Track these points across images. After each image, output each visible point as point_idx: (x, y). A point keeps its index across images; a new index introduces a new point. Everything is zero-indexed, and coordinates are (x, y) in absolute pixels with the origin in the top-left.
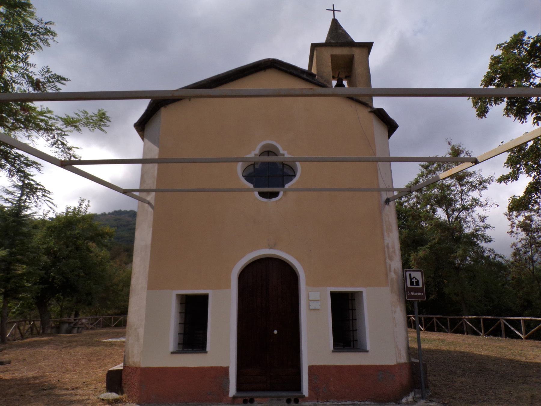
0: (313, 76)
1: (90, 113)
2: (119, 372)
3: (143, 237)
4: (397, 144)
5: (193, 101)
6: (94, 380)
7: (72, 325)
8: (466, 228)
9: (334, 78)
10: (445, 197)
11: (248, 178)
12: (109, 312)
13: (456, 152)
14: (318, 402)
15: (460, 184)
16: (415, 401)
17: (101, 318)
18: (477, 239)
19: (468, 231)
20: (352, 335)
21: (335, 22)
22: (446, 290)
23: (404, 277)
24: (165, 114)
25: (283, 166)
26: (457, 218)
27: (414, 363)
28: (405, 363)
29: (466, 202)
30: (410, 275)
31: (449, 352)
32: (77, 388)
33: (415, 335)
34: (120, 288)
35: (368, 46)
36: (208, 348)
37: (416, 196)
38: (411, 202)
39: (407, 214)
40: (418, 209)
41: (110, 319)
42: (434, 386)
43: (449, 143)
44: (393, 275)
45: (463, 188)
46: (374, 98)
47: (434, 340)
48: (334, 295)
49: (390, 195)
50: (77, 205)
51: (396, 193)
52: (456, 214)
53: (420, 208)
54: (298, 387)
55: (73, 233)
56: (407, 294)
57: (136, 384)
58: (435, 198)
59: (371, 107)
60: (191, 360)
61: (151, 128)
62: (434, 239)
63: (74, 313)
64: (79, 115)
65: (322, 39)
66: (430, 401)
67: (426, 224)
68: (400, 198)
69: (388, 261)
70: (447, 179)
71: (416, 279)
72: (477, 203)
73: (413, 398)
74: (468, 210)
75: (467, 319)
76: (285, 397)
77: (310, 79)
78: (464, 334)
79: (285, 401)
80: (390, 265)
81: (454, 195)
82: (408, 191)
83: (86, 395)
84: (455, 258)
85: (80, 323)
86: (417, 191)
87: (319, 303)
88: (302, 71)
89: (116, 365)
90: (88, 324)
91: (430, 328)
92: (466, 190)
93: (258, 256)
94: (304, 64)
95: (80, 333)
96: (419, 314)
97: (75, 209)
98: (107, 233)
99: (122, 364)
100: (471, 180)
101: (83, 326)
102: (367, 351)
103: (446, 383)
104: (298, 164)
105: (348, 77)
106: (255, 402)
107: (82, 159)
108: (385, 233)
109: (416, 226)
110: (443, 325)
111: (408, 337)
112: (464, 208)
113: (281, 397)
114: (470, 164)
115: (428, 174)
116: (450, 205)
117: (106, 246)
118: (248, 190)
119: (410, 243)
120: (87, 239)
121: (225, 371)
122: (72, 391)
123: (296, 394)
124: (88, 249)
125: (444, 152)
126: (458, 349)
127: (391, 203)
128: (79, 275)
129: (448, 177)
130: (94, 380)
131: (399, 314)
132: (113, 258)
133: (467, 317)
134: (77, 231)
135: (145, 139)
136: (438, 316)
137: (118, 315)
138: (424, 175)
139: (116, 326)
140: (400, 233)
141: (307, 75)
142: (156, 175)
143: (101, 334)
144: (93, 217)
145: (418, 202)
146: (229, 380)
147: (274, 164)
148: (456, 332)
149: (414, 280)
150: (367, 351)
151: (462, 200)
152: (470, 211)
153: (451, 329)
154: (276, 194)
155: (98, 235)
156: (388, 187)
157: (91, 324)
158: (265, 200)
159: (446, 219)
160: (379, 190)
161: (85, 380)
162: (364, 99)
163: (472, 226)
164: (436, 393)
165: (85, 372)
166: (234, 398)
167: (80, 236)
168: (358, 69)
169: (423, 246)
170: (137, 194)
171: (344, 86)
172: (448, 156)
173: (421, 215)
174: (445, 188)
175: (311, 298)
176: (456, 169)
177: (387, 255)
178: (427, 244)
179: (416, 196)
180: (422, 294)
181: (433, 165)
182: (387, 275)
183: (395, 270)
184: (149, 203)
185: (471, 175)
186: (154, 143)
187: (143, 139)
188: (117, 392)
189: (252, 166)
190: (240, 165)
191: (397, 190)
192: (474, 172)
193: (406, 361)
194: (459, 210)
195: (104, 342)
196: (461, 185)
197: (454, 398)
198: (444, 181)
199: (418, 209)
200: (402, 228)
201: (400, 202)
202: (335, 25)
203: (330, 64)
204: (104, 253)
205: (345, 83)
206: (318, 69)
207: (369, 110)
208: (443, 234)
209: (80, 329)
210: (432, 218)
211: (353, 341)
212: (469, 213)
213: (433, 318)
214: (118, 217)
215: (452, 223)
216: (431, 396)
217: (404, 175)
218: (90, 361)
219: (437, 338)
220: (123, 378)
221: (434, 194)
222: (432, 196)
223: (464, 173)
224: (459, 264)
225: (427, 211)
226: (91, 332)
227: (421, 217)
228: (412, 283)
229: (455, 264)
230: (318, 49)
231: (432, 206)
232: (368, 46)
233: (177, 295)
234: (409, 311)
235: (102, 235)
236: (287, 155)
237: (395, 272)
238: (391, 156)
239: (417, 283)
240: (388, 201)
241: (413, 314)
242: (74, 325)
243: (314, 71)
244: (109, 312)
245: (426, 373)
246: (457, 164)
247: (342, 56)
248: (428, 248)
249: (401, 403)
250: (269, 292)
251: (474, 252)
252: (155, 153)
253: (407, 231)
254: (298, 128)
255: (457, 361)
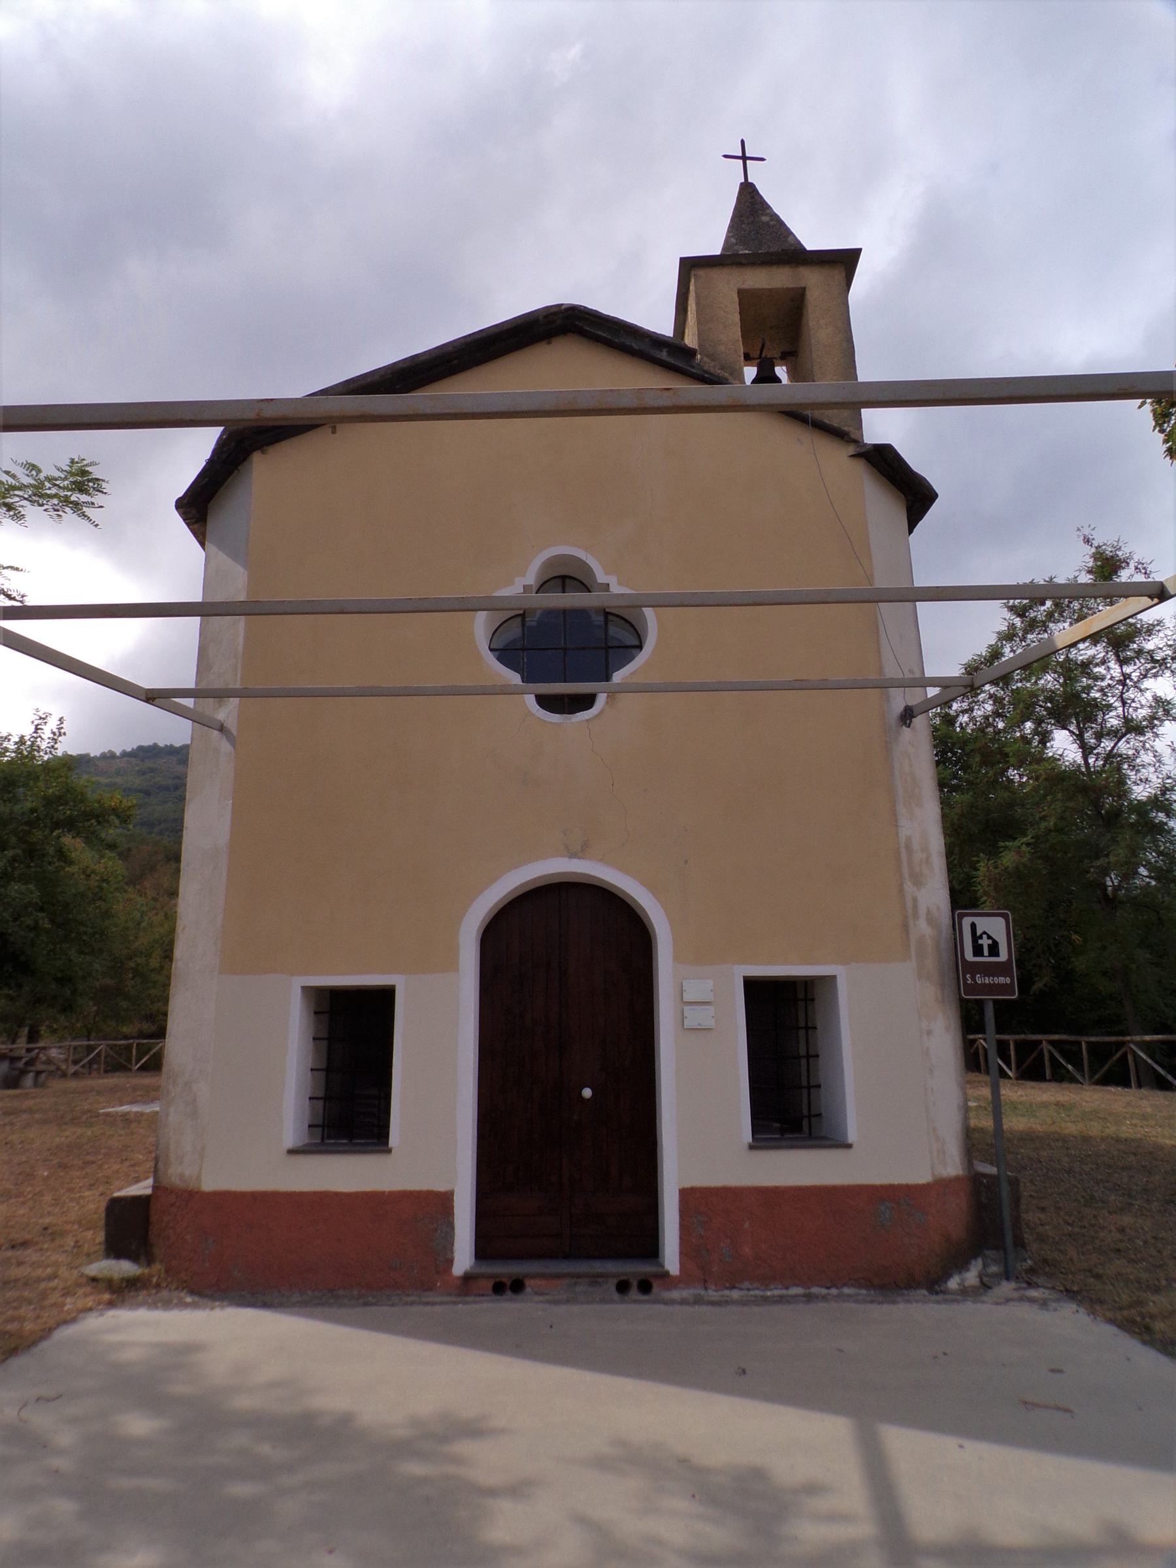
0: (690, 353)
1: (48, 470)
2: (141, 1203)
3: (207, 824)
4: (932, 552)
5: (350, 432)
6: (73, 1223)
7: (20, 1064)
8: (1135, 783)
9: (748, 358)
10: (1077, 696)
11: (506, 654)
12: (125, 1030)
13: (1107, 565)
14: (706, 1289)
15: (1118, 656)
16: (985, 1286)
17: (102, 1046)
18: (1168, 816)
19: (1140, 793)
20: (805, 1101)
21: (748, 192)
22: (1080, 964)
23: (954, 929)
24: (264, 471)
25: (606, 621)
26: (1110, 756)
27: (984, 1175)
28: (957, 1179)
29: (1136, 709)
30: (973, 926)
31: (1086, 1139)
32: (25, 1244)
33: (986, 1092)
34: (154, 963)
35: (845, 261)
36: (394, 1139)
37: (991, 696)
38: (978, 713)
39: (968, 749)
40: (1000, 731)
41: (128, 1048)
42: (1042, 1239)
43: (1087, 541)
44: (922, 928)
45: (1128, 669)
46: (865, 412)
47: (1045, 1105)
48: (753, 987)
49: (914, 697)
50: (28, 731)
51: (932, 692)
52: (1107, 744)
53: (1004, 730)
54: (651, 1249)
55: (17, 808)
56: (965, 980)
57: (188, 1237)
58: (1049, 699)
59: (857, 442)
60: (347, 1173)
61: (223, 517)
62: (1044, 818)
63: (26, 1030)
64: (14, 476)
65: (713, 244)
66: (1030, 1285)
67: (1021, 776)
68: (947, 704)
69: (909, 887)
70: (1081, 646)
71: (989, 937)
72: (1167, 712)
73: (980, 1276)
74: (1142, 733)
75: (1138, 1043)
76: (614, 1276)
77: (679, 363)
78: (1130, 1087)
79: (613, 1288)
80: (915, 900)
81: (1101, 690)
82: (969, 684)
83: (48, 1266)
84: (1105, 872)
85: (43, 1057)
86: (994, 682)
87: (711, 1009)
88: (656, 341)
89: (137, 1180)
90: (66, 1060)
91: (1032, 1072)
92: (1135, 676)
93: (534, 880)
94: (661, 322)
95: (43, 1085)
96: (1000, 1030)
97: (22, 741)
98: (114, 810)
99: (150, 1181)
100: (1149, 646)
101: (52, 1068)
102: (849, 1146)
103: (1076, 1230)
104: (648, 612)
105: (790, 356)
106: (528, 1290)
107: (31, 601)
108: (901, 809)
109: (993, 784)
110: (1069, 1062)
111: (966, 1100)
112: (1132, 727)
113: (601, 1275)
114: (1146, 601)
115: (1026, 632)
116: (1091, 718)
117: (112, 847)
118: (506, 690)
119: (975, 832)
120: (57, 825)
121: (443, 1202)
122: (10, 1253)
123: (643, 1268)
124: (62, 855)
125: (1071, 565)
126: (1111, 1130)
127: (919, 722)
128: (35, 928)
129: (1083, 640)
130: (73, 1223)
131: (942, 1039)
132: (134, 880)
133: (1137, 1038)
134: (29, 805)
135: (207, 543)
136: (1056, 1037)
137: (150, 1037)
138: (1015, 635)
139: (143, 1068)
140: (945, 803)
141: (669, 353)
142: (240, 648)
143: (99, 1093)
144: (71, 763)
145: (997, 714)
146: (453, 1229)
147: (580, 614)
148: (1106, 1081)
149: (985, 942)
150: (849, 1146)
151: (1124, 703)
152: (1149, 735)
153: (1093, 1072)
154: (587, 701)
155: (90, 815)
156: (908, 675)
157: (75, 1062)
158: (555, 718)
159: (1079, 759)
160: (884, 685)
161: (47, 1221)
162: (833, 418)
163: (1153, 777)
164: (1045, 1261)
165: (48, 1198)
166: (468, 1278)
167: (38, 818)
168: (818, 330)
169: (1013, 838)
170: (188, 702)
171: (778, 380)
172: (1085, 579)
173: (1007, 750)
174: (1073, 671)
175: (688, 997)
176: (1105, 616)
177: (906, 876)
178: (1026, 836)
179: (991, 696)
180: (1008, 980)
181: (1043, 604)
182: (906, 928)
183: (928, 911)
184: (222, 729)
185: (1150, 630)
186: (235, 555)
187: (202, 544)
188: (134, 1258)
189: (519, 619)
190: (481, 616)
191: (934, 682)
192: (1160, 623)
193: (961, 1172)
194: (1117, 735)
195: (108, 1115)
196: (1122, 662)
197: (1098, 1277)
198: (1074, 651)
199: (998, 732)
200: (954, 789)
201: (948, 714)
202: (750, 204)
203: (737, 318)
204: (112, 865)
205: (781, 371)
206: (700, 334)
207: (852, 449)
208: (1071, 804)
209: (43, 1077)
210: (1040, 759)
211: (809, 1116)
212: (1144, 742)
213: (1040, 1042)
214: (148, 764)
215: (1096, 772)
216: (1032, 1271)
217: (955, 640)
218: (64, 1167)
219: (1053, 1099)
220: (154, 1218)
221: (1043, 690)
222: (1036, 696)
223: (1131, 625)
224: (1116, 889)
225: (1023, 737)
226: (73, 1084)
227: (1007, 755)
228: (978, 950)
229: (1105, 887)
230: (701, 273)
231: (1039, 722)
232: (845, 261)
233: (306, 990)
234: (970, 1020)
235: (100, 816)
236: (616, 589)
237: (930, 920)
238: (916, 585)
239: (994, 949)
240: (908, 715)
241: (984, 1032)
242: (27, 1064)
243: (690, 340)
244: (125, 1030)
245: (1016, 1200)
246: (1110, 599)
247: (772, 294)
248: (1028, 844)
249: (943, 1292)
250: (568, 975)
251: (1160, 853)
252: (237, 588)
253: (967, 797)
254: (647, 505)
255: (1110, 1167)
